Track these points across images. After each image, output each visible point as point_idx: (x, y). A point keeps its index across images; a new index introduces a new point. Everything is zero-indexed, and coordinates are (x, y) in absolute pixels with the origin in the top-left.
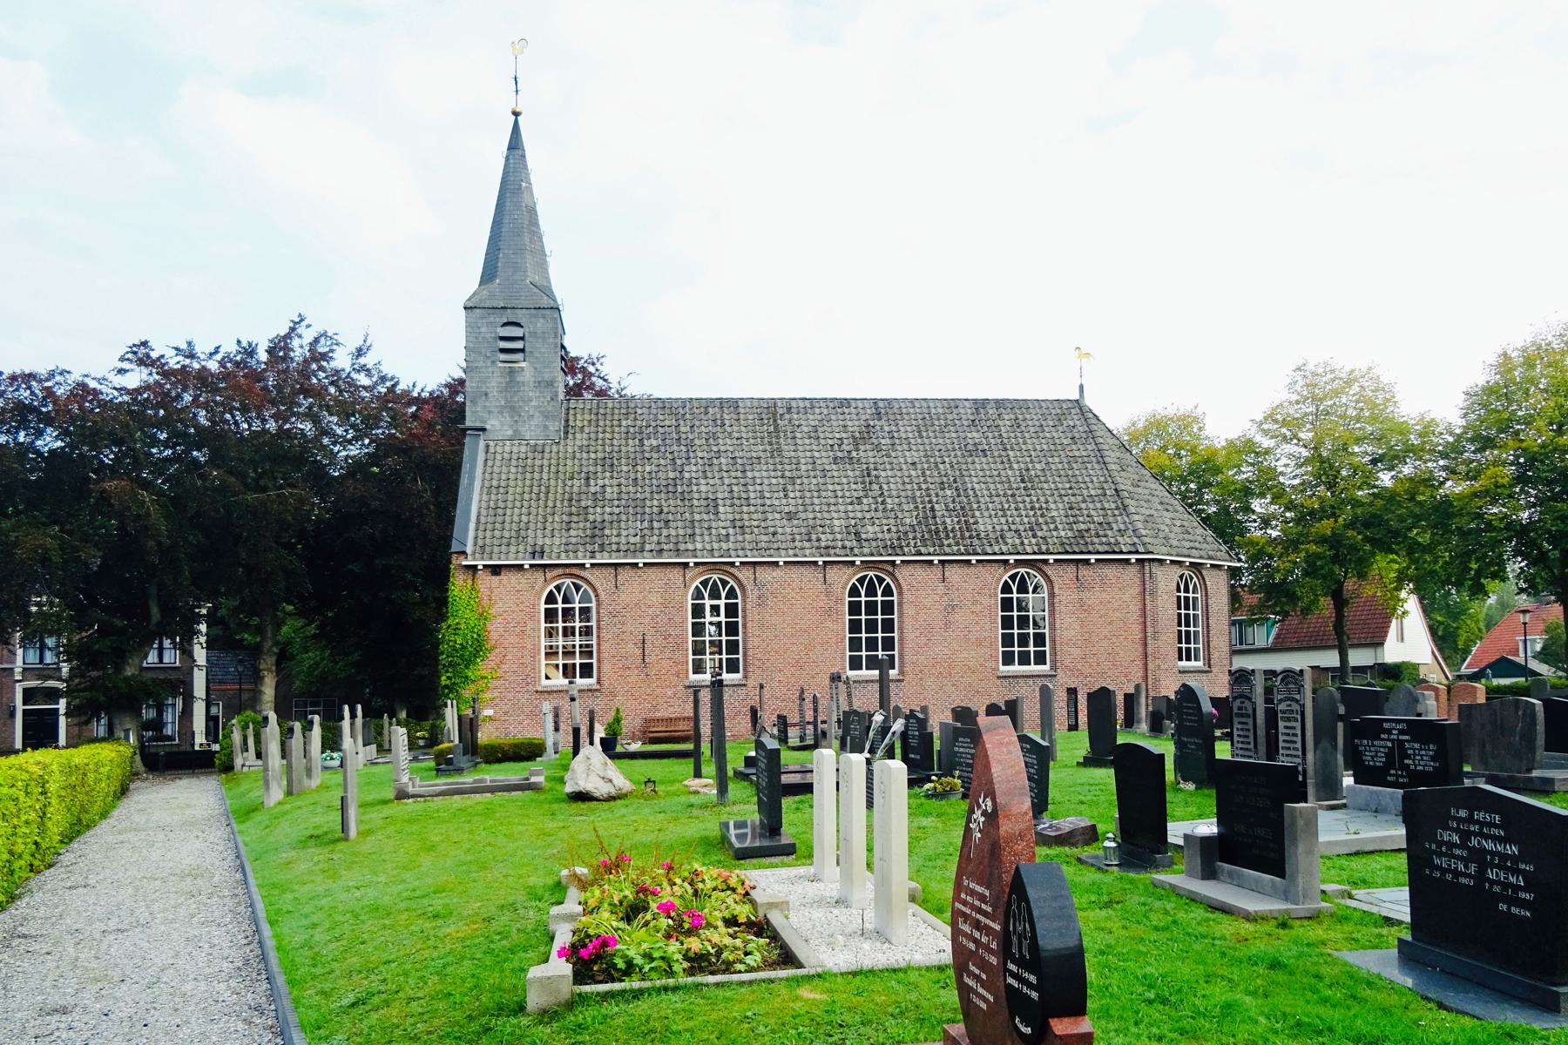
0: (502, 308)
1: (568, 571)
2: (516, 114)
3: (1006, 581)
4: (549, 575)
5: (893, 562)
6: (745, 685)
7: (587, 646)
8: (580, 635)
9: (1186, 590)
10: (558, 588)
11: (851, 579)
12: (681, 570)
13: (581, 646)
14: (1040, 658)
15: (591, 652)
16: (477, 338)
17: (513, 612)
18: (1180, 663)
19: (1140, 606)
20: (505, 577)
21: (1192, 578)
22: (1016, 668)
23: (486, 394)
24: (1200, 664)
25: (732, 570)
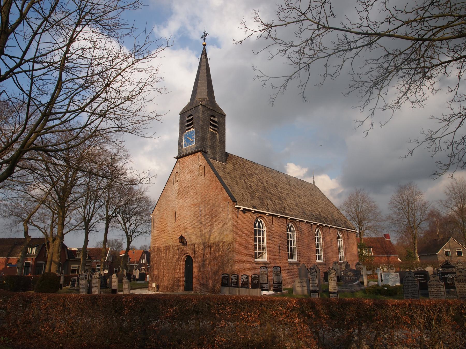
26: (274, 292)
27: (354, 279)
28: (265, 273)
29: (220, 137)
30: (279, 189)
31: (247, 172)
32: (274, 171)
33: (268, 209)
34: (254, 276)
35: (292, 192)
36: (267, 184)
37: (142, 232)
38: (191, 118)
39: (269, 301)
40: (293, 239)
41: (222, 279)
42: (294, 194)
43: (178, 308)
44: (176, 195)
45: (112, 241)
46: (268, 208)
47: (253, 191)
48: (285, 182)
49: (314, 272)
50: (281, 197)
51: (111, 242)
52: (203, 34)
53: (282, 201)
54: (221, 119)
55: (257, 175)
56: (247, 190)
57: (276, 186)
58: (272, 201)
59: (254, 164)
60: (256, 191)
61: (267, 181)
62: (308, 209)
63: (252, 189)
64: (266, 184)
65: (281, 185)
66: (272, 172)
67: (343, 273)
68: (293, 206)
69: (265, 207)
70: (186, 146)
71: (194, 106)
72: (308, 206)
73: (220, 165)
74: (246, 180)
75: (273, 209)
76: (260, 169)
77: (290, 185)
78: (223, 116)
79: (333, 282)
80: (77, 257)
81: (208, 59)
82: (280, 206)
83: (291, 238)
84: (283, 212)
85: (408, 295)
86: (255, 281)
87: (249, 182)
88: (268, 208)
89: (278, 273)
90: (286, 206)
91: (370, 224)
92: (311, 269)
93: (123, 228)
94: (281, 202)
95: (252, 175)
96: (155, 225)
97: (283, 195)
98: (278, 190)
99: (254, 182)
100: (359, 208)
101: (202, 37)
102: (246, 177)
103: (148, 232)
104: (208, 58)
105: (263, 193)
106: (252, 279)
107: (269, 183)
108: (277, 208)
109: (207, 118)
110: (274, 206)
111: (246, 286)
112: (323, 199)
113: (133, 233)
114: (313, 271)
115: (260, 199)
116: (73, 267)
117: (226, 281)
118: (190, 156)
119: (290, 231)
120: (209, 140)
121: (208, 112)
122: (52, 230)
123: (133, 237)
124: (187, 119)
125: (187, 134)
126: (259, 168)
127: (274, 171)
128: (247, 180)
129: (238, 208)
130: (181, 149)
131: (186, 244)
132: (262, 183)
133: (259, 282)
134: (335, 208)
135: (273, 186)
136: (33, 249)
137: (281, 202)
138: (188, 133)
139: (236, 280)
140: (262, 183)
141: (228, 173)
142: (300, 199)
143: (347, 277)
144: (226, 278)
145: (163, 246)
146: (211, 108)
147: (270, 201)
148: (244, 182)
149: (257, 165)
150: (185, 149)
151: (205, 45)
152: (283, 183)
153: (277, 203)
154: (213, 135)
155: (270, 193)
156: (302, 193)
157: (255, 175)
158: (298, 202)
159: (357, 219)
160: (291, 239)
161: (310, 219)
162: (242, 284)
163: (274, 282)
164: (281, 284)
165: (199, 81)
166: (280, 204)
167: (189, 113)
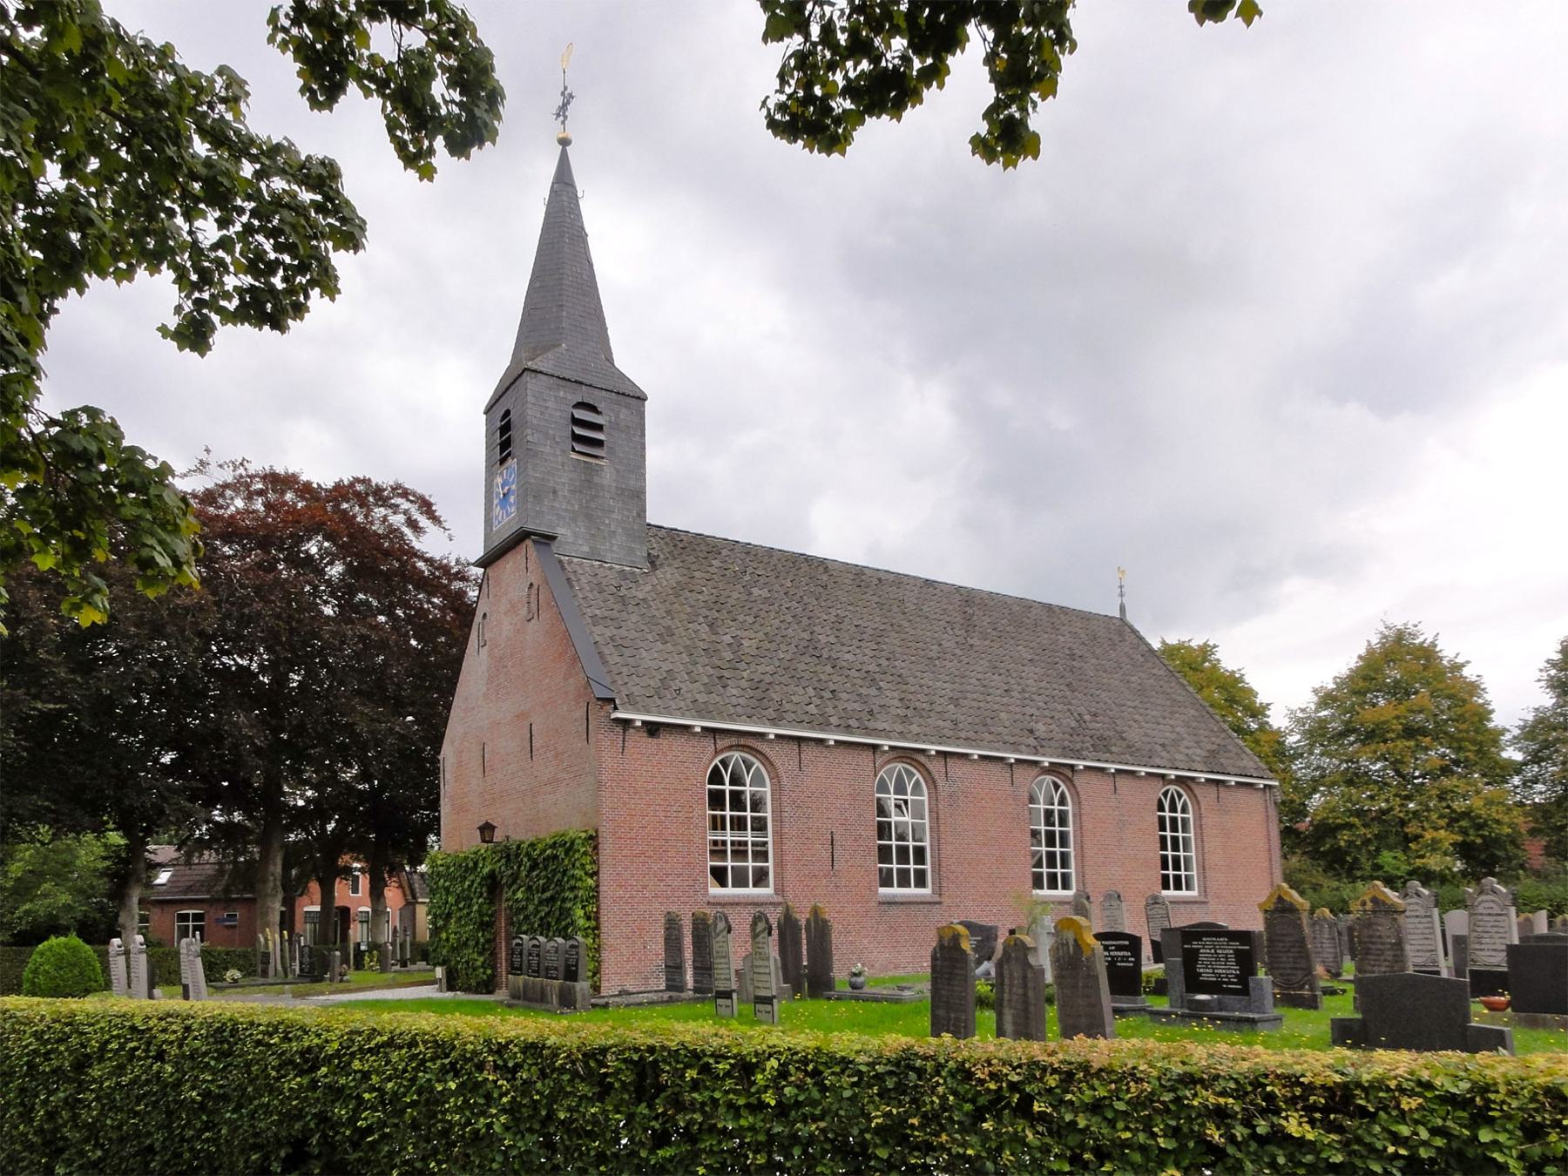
0: (576, 382)
1: (743, 741)
2: (564, 142)
3: (716, 766)
4: (721, 743)
5: (1072, 767)
6: (940, 903)
7: (740, 843)
8: (732, 829)
9: (1173, 809)
10: (724, 763)
11: (712, 760)
12: (871, 753)
13: (733, 843)
14: (921, 880)
15: (766, 853)
16: (542, 413)
17: (676, 790)
18: (1165, 893)
19: (1265, 832)
20: (665, 741)
21: (1180, 796)
22: (895, 891)
23: (555, 492)
24: (1194, 893)
25: (922, 759)
121: (562, 394)
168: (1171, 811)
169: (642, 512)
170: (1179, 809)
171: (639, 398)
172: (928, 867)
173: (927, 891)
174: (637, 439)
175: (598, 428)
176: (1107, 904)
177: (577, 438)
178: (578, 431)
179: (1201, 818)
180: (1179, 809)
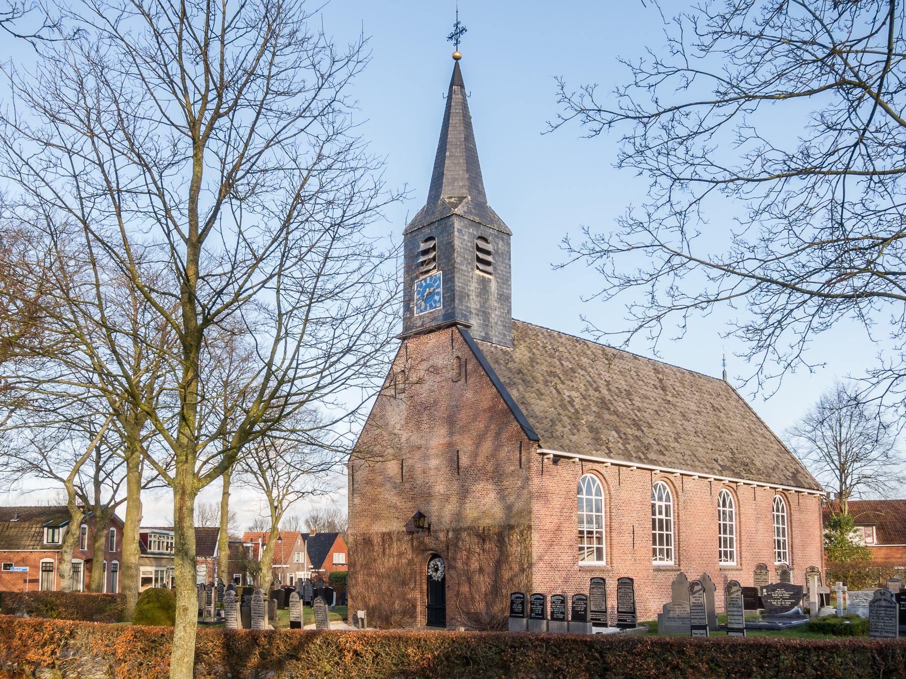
2: (457, 59)
9: (589, 492)
24: (734, 564)
26: (617, 630)
27: (788, 603)
28: (600, 590)
29: (499, 288)
30: (637, 402)
31: (562, 365)
32: (627, 355)
33: (610, 452)
34: (577, 597)
35: (666, 406)
36: (609, 390)
37: (303, 493)
38: (431, 244)
39: (608, 644)
40: (667, 516)
41: (512, 602)
42: (672, 411)
43: (442, 654)
44: (403, 422)
45: (211, 506)
46: (608, 449)
47: (577, 412)
48: (653, 382)
49: (700, 590)
50: (640, 420)
51: (208, 509)
52: (453, 30)
53: (643, 431)
54: (501, 243)
55: (586, 371)
56: (561, 411)
57: (629, 394)
58: (618, 432)
59: (578, 341)
60: (583, 410)
61: (608, 384)
62: (703, 445)
63: (573, 406)
64: (604, 391)
65: (642, 392)
66: (622, 357)
67: (767, 592)
68: (667, 441)
69: (603, 447)
70: (421, 311)
71: (438, 216)
72: (705, 437)
73: (500, 353)
74: (560, 386)
75: (620, 451)
76: (593, 353)
77: (664, 389)
78: (505, 237)
79: (735, 609)
80: (150, 549)
81: (468, 93)
82: (638, 443)
83: (660, 513)
84: (643, 457)
85: (877, 634)
86: (580, 607)
87: (565, 391)
88: (608, 449)
89: (628, 590)
90: (652, 441)
91: (867, 471)
92: (693, 584)
93: (260, 483)
94: (639, 433)
95: (573, 370)
96: (355, 486)
97: (646, 415)
98: (633, 404)
99: (577, 390)
100: (844, 430)
101: (451, 38)
102: (560, 378)
103: (319, 492)
104: (467, 91)
105: (598, 416)
106: (573, 603)
107: (613, 389)
108: (629, 447)
109: (470, 244)
110: (624, 445)
111: (561, 616)
112: (743, 418)
113: (284, 496)
114: (697, 588)
115: (591, 429)
116: (144, 573)
117: (520, 607)
118: (432, 335)
119: (660, 499)
120: (473, 296)
121: (471, 230)
122: (98, 491)
123: (285, 503)
124: (423, 246)
125: (423, 282)
126: (589, 352)
127: (627, 355)
128: (561, 386)
129: (543, 454)
130: (410, 318)
131: (429, 529)
132: (596, 390)
133: (588, 610)
134: (773, 438)
135: (623, 394)
136: (56, 531)
137: (639, 433)
138: (425, 280)
139: (540, 605)
140: (596, 390)
141: (520, 372)
142: (686, 423)
143: (775, 599)
144: (520, 601)
145: (377, 534)
146: (477, 219)
147: (614, 433)
148: (554, 391)
149: (585, 344)
150: (420, 317)
151: (457, 59)
152: (646, 384)
153: (630, 437)
154: (484, 283)
155: (616, 413)
156: (694, 407)
157: (580, 370)
158: (680, 429)
159: (836, 458)
160: (660, 517)
161: (706, 469)
162: (552, 613)
163: (620, 610)
164: (606, 612)
165: (448, 154)
166: (637, 438)
167: (427, 232)
168: (596, 495)
169: (509, 312)
170: (594, 491)
171: (508, 234)
172: (604, 546)
173: (602, 563)
174: (507, 261)
175: (488, 253)
176: (758, 571)
177: (479, 260)
178: (481, 256)
179: (791, 516)
180: (594, 491)
